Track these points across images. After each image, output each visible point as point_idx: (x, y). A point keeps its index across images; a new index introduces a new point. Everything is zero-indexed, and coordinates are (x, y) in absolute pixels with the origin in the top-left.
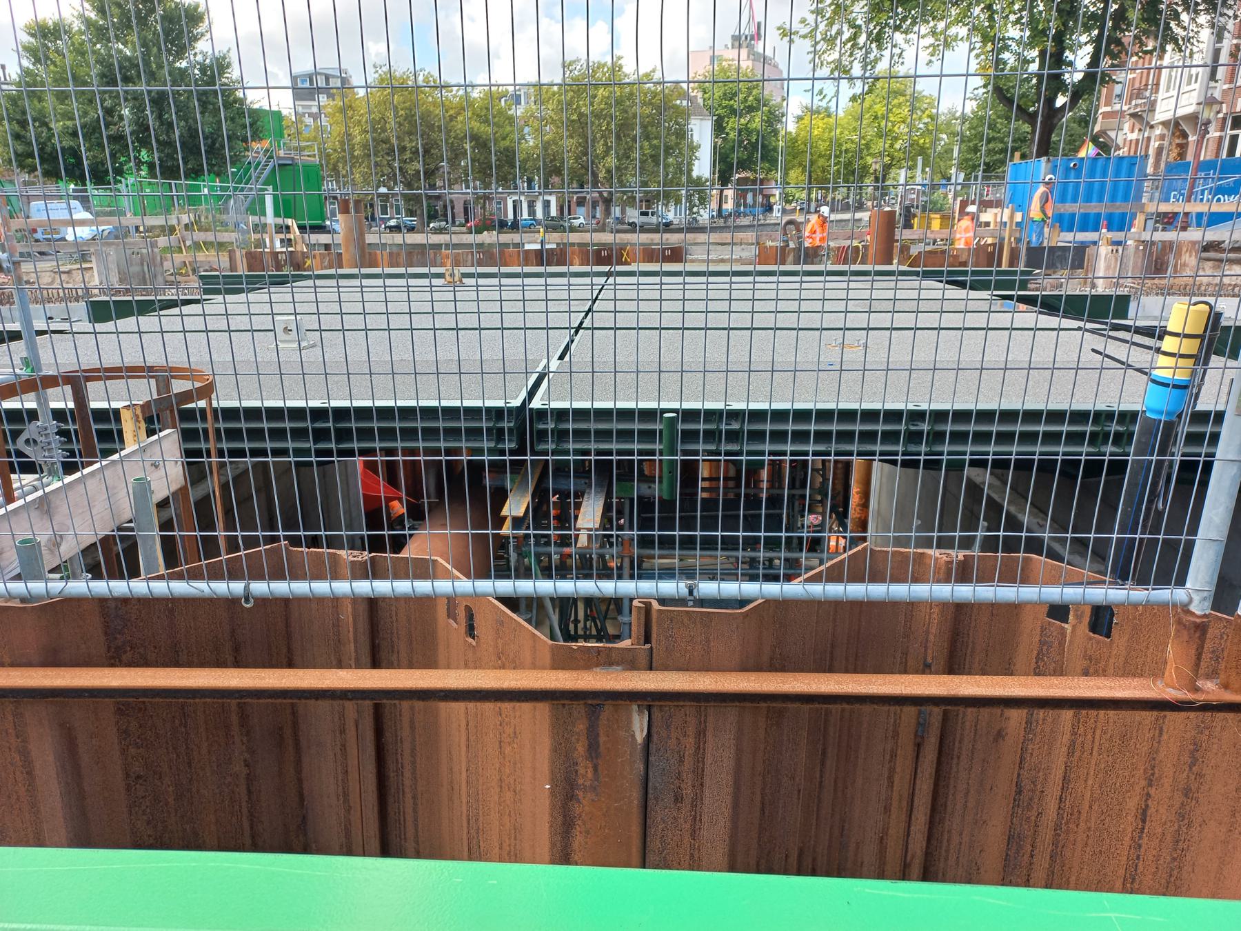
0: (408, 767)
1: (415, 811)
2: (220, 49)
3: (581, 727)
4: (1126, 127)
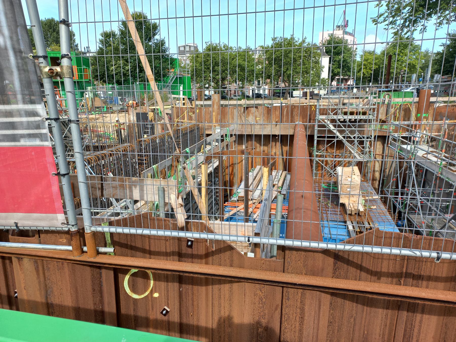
2: (162, 37)
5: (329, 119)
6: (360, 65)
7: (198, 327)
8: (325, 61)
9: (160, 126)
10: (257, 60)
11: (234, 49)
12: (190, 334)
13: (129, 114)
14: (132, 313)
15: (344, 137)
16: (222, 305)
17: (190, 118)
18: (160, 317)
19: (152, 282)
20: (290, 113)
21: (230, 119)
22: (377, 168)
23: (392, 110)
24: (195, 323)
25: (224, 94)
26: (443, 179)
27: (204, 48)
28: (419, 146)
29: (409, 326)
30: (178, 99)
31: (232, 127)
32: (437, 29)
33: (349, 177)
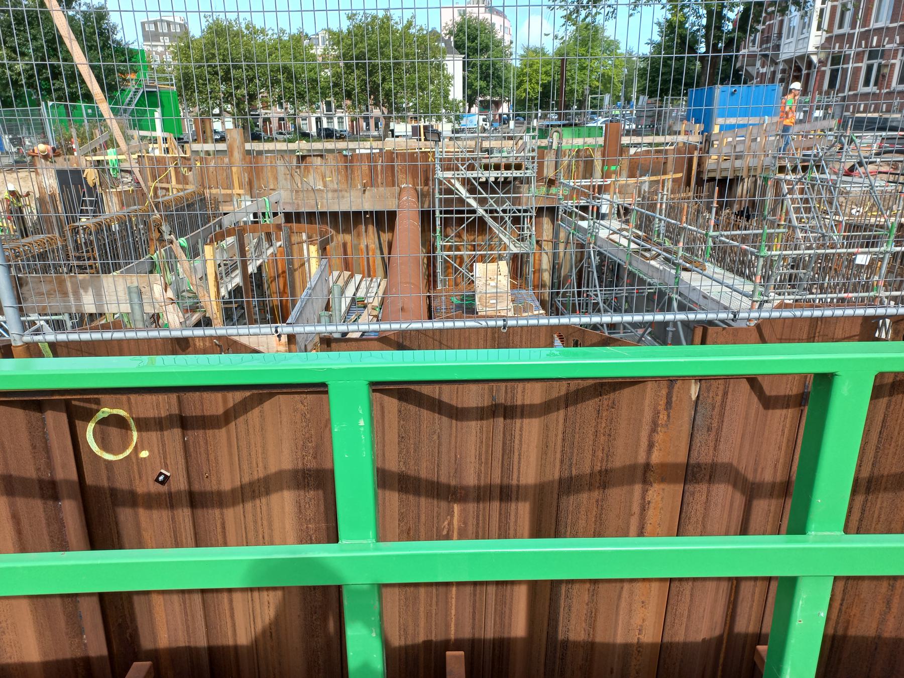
0: (517, 437)
1: (519, 463)
3: (664, 392)
4: (758, 63)
5: (458, 179)
6: (521, 74)
7: (220, 494)
8: (454, 66)
9: (115, 199)
10: (321, 59)
11: (270, 32)
12: (207, 507)
13: (37, 173)
14: (105, 483)
15: (486, 211)
16: (252, 441)
17: (182, 179)
18: (155, 488)
19: (135, 434)
20: (387, 168)
21: (271, 181)
22: (546, 264)
23: (566, 161)
24: (215, 488)
25: (257, 129)
26: (634, 275)
27: (203, 27)
28: (602, 222)
29: (508, 438)
30: (155, 140)
31: (274, 196)
32: (631, 15)
33: (491, 279)
